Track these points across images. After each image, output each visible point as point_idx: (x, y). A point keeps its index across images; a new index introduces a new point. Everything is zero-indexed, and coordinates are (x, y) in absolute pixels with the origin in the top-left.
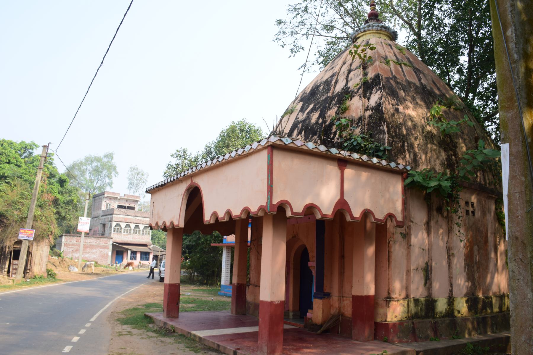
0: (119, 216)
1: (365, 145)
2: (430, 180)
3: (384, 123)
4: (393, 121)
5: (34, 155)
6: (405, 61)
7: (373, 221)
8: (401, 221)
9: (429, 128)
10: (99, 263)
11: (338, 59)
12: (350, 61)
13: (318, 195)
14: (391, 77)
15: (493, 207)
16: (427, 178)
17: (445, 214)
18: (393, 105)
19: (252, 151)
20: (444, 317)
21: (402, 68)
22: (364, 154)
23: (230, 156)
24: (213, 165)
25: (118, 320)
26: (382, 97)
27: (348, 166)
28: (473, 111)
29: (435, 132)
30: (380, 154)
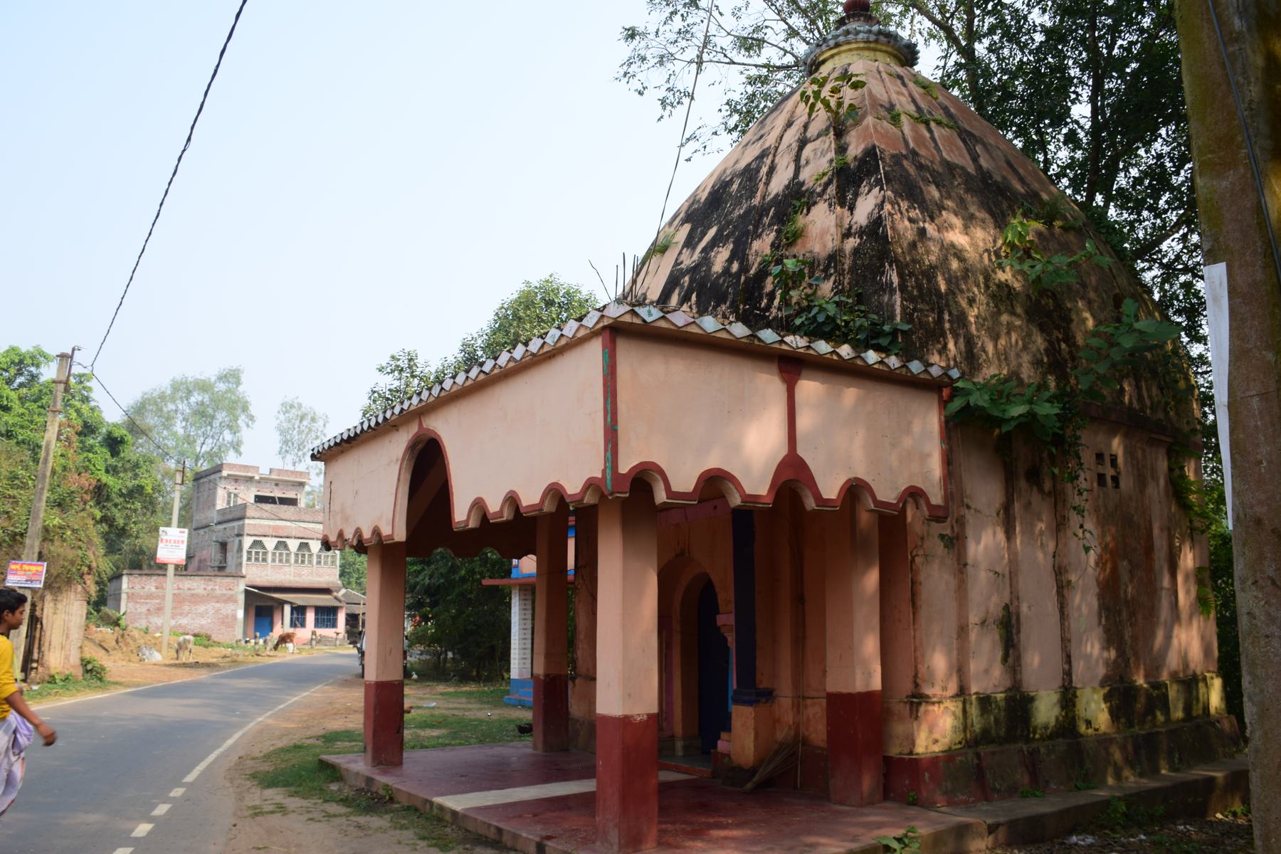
0: (258, 522)
1: (847, 323)
2: (1009, 401)
3: (891, 266)
4: (914, 261)
5: (42, 379)
6: (939, 115)
7: (872, 506)
8: (939, 506)
9: (1004, 276)
10: (214, 637)
11: (775, 114)
12: (805, 118)
13: (736, 447)
14: (904, 152)
15: (1163, 465)
16: (1000, 397)
17: (1047, 486)
18: (911, 220)
19: (563, 342)
20: (1052, 736)
21: (930, 131)
22: (844, 343)
23: (512, 359)
24: (469, 382)
25: (254, 776)
26: (883, 202)
27: (804, 373)
28: (1108, 232)
30: (884, 342)
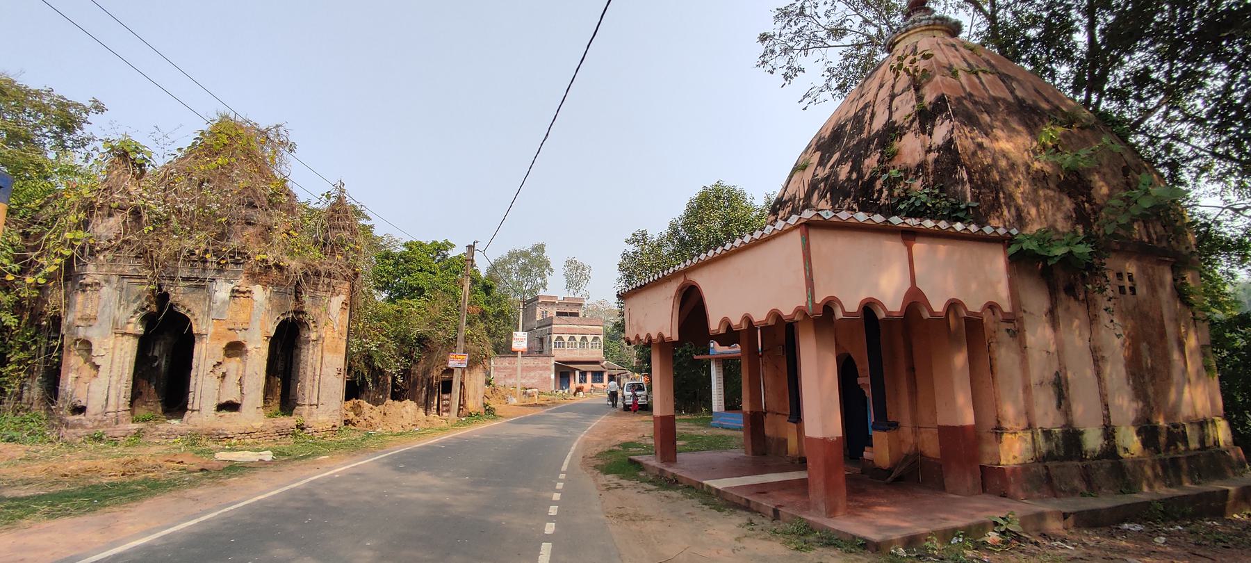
0: (559, 326)
1: (934, 205)
2: (1051, 246)
9: (1037, 165)
12: (892, 81)
15: (1168, 278)
17: (1081, 297)
20: (1098, 458)
21: (979, 78)
29: (1048, 169)
30: (961, 215)
